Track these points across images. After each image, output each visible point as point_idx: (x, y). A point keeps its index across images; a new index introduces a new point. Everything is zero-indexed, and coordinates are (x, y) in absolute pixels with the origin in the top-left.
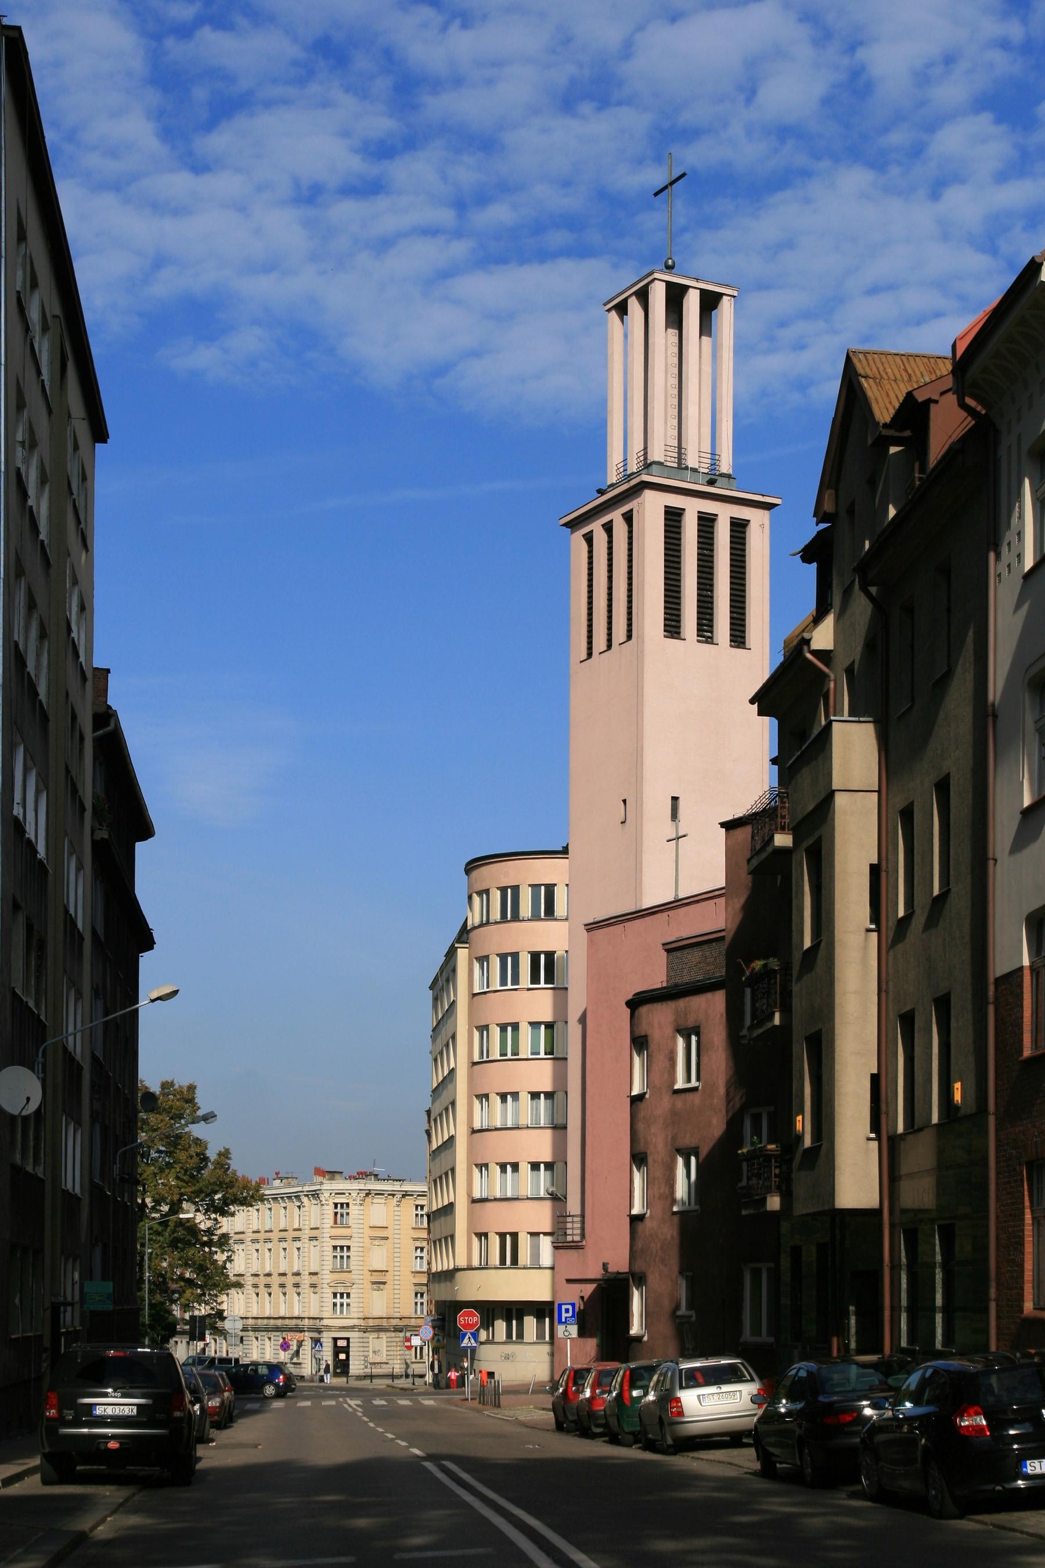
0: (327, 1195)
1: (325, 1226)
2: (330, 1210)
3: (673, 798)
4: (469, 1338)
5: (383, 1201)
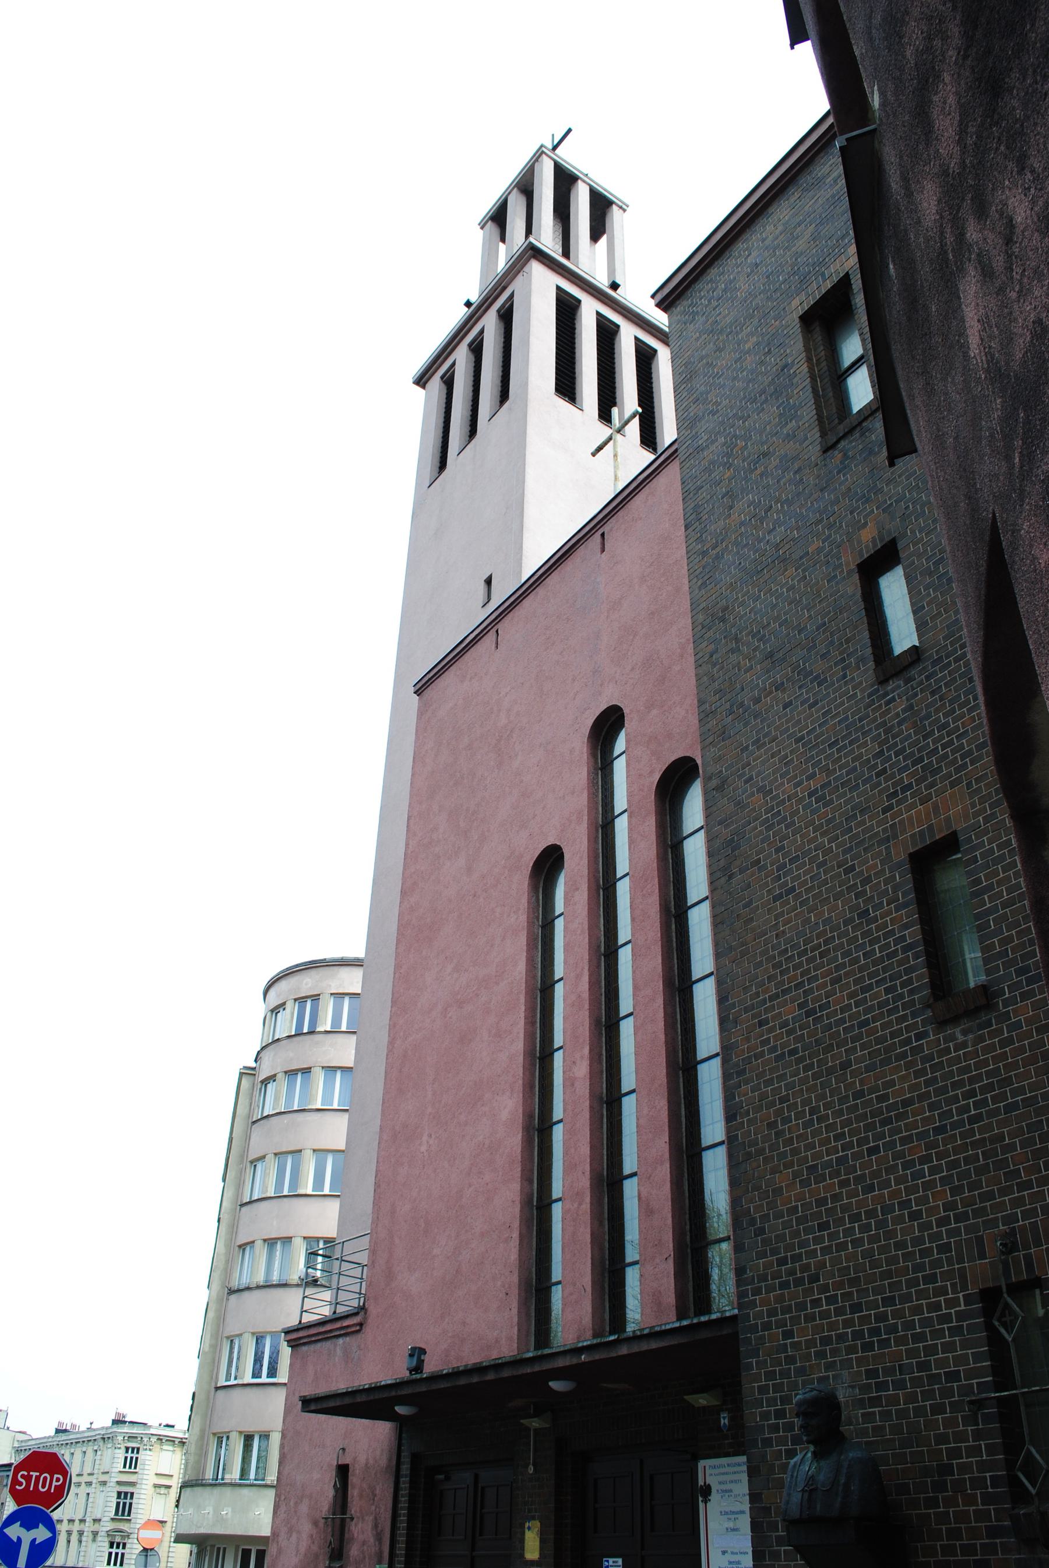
0: (120, 1438)
1: (114, 1470)
2: (121, 1454)
3: (594, 456)
5: (171, 1448)
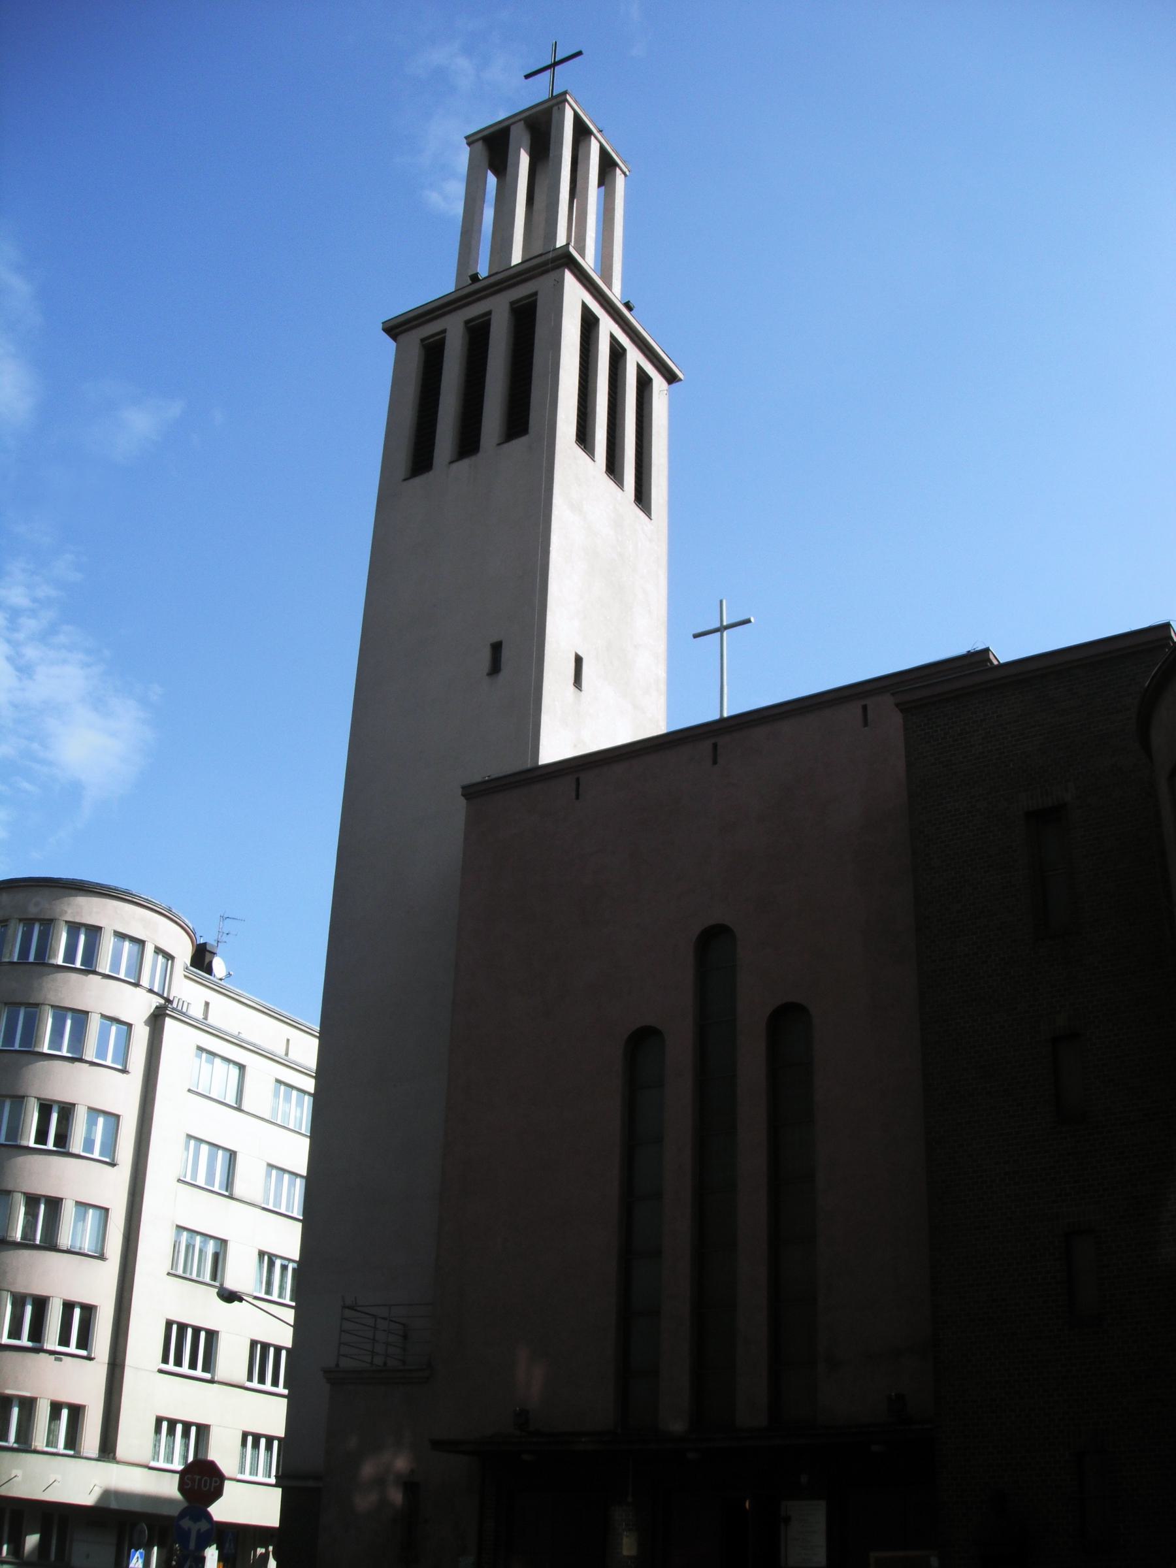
4: (138, 1558)
